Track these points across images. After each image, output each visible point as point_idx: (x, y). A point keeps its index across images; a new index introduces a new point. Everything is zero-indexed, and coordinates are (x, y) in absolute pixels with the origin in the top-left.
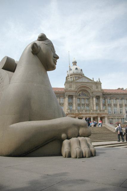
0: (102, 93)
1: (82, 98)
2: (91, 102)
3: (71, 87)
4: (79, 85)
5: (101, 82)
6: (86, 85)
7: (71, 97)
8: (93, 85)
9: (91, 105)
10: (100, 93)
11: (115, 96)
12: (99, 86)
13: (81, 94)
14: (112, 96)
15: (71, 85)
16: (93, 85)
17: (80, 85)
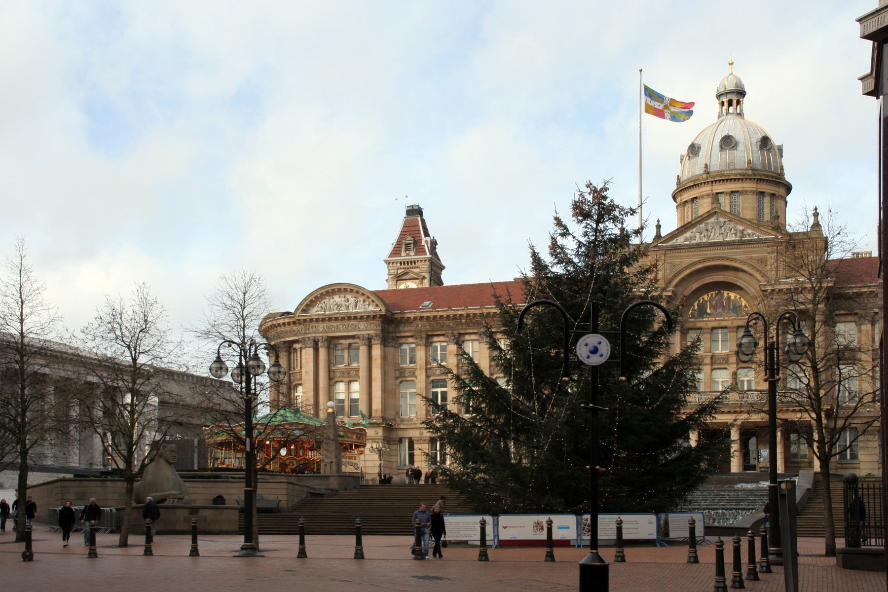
1: (715, 324)
4: (687, 261)
6: (713, 259)
13: (712, 307)
17: (695, 263)
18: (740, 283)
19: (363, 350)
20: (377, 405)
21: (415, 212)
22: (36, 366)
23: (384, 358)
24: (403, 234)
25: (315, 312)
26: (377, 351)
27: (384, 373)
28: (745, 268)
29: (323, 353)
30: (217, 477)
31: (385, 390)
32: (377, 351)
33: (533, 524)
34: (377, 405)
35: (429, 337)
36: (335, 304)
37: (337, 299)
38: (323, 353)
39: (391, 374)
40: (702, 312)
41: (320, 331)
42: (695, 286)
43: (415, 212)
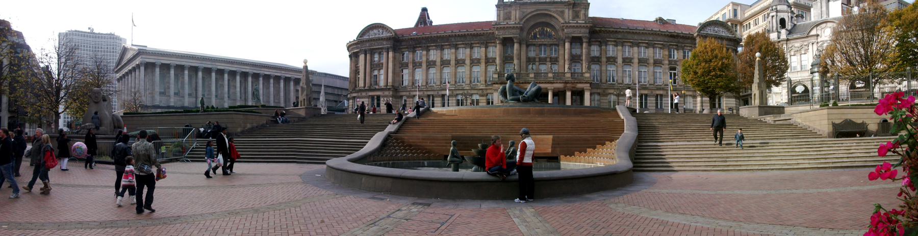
0: (588, 31)
2: (561, 52)
3: (508, 17)
4: (529, 11)
5: (495, 9)
7: (507, 42)
8: (567, 11)
9: (561, 62)
10: (583, 30)
11: (629, 36)
12: (583, 12)
14: (619, 36)
15: (510, 13)
16: (567, 11)
18: (552, 23)
19: (385, 54)
20: (390, 80)
21: (424, 10)
22: (315, 80)
23: (394, 58)
24: (420, 19)
25: (366, 37)
26: (391, 54)
27: (394, 65)
28: (555, 15)
29: (368, 56)
30: (252, 112)
31: (394, 73)
32: (391, 54)
33: (658, 17)
34: (390, 80)
35: (414, 48)
36: (373, 34)
37: (375, 31)
38: (368, 56)
39: (398, 65)
40: (535, 37)
41: (367, 46)
42: (532, 23)
43: (424, 10)
